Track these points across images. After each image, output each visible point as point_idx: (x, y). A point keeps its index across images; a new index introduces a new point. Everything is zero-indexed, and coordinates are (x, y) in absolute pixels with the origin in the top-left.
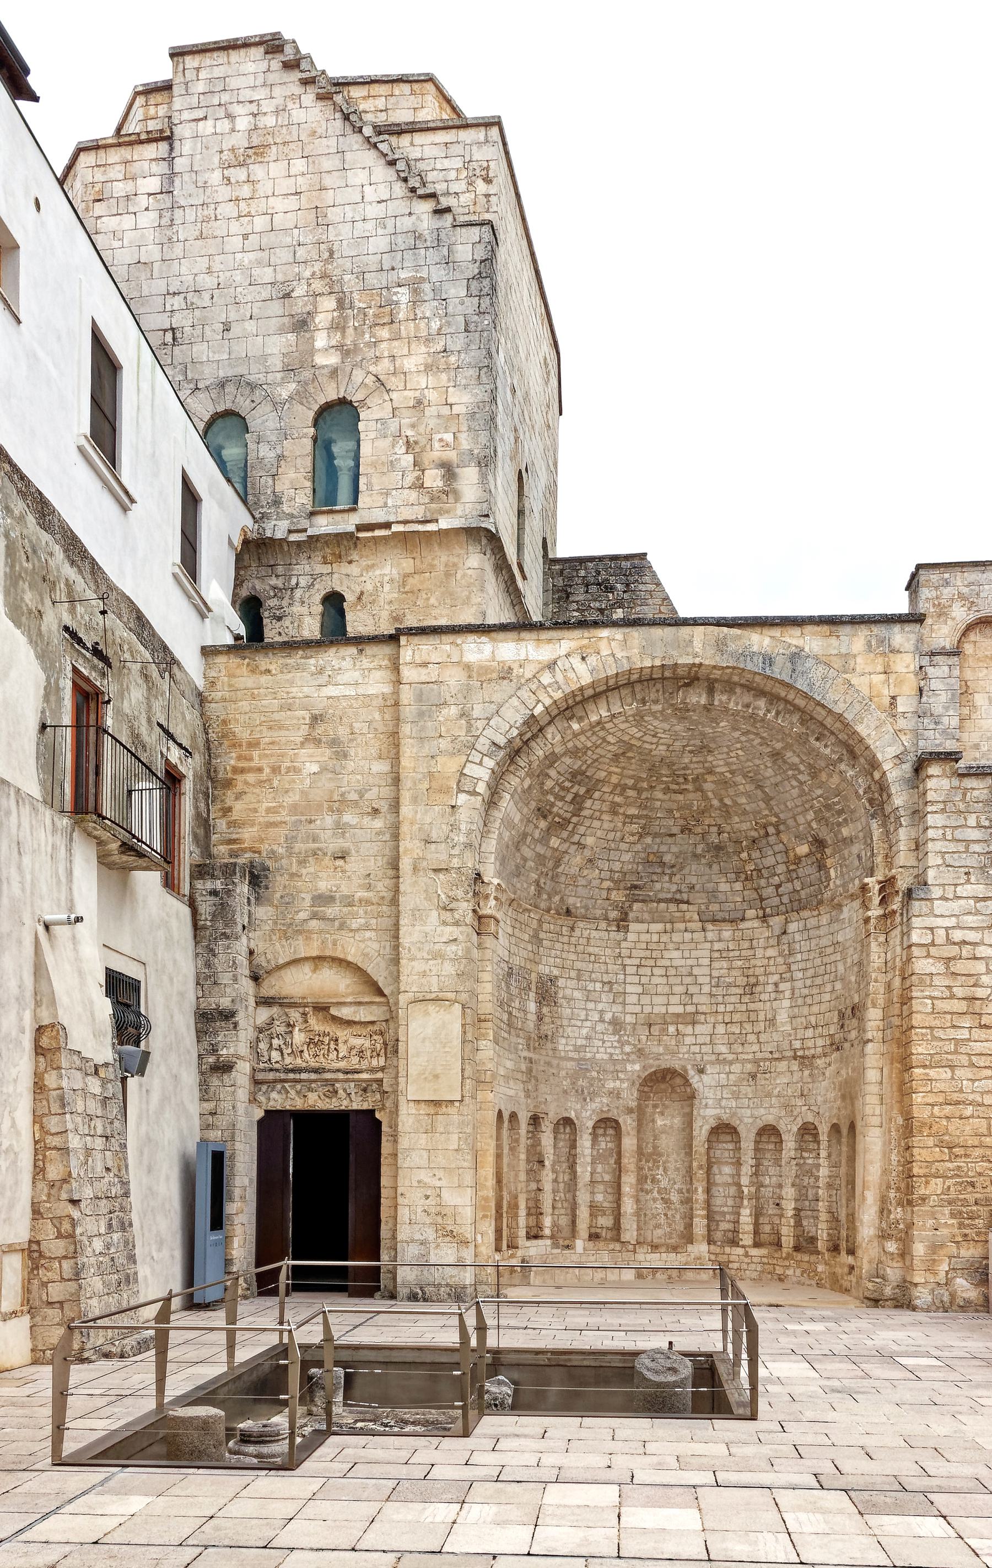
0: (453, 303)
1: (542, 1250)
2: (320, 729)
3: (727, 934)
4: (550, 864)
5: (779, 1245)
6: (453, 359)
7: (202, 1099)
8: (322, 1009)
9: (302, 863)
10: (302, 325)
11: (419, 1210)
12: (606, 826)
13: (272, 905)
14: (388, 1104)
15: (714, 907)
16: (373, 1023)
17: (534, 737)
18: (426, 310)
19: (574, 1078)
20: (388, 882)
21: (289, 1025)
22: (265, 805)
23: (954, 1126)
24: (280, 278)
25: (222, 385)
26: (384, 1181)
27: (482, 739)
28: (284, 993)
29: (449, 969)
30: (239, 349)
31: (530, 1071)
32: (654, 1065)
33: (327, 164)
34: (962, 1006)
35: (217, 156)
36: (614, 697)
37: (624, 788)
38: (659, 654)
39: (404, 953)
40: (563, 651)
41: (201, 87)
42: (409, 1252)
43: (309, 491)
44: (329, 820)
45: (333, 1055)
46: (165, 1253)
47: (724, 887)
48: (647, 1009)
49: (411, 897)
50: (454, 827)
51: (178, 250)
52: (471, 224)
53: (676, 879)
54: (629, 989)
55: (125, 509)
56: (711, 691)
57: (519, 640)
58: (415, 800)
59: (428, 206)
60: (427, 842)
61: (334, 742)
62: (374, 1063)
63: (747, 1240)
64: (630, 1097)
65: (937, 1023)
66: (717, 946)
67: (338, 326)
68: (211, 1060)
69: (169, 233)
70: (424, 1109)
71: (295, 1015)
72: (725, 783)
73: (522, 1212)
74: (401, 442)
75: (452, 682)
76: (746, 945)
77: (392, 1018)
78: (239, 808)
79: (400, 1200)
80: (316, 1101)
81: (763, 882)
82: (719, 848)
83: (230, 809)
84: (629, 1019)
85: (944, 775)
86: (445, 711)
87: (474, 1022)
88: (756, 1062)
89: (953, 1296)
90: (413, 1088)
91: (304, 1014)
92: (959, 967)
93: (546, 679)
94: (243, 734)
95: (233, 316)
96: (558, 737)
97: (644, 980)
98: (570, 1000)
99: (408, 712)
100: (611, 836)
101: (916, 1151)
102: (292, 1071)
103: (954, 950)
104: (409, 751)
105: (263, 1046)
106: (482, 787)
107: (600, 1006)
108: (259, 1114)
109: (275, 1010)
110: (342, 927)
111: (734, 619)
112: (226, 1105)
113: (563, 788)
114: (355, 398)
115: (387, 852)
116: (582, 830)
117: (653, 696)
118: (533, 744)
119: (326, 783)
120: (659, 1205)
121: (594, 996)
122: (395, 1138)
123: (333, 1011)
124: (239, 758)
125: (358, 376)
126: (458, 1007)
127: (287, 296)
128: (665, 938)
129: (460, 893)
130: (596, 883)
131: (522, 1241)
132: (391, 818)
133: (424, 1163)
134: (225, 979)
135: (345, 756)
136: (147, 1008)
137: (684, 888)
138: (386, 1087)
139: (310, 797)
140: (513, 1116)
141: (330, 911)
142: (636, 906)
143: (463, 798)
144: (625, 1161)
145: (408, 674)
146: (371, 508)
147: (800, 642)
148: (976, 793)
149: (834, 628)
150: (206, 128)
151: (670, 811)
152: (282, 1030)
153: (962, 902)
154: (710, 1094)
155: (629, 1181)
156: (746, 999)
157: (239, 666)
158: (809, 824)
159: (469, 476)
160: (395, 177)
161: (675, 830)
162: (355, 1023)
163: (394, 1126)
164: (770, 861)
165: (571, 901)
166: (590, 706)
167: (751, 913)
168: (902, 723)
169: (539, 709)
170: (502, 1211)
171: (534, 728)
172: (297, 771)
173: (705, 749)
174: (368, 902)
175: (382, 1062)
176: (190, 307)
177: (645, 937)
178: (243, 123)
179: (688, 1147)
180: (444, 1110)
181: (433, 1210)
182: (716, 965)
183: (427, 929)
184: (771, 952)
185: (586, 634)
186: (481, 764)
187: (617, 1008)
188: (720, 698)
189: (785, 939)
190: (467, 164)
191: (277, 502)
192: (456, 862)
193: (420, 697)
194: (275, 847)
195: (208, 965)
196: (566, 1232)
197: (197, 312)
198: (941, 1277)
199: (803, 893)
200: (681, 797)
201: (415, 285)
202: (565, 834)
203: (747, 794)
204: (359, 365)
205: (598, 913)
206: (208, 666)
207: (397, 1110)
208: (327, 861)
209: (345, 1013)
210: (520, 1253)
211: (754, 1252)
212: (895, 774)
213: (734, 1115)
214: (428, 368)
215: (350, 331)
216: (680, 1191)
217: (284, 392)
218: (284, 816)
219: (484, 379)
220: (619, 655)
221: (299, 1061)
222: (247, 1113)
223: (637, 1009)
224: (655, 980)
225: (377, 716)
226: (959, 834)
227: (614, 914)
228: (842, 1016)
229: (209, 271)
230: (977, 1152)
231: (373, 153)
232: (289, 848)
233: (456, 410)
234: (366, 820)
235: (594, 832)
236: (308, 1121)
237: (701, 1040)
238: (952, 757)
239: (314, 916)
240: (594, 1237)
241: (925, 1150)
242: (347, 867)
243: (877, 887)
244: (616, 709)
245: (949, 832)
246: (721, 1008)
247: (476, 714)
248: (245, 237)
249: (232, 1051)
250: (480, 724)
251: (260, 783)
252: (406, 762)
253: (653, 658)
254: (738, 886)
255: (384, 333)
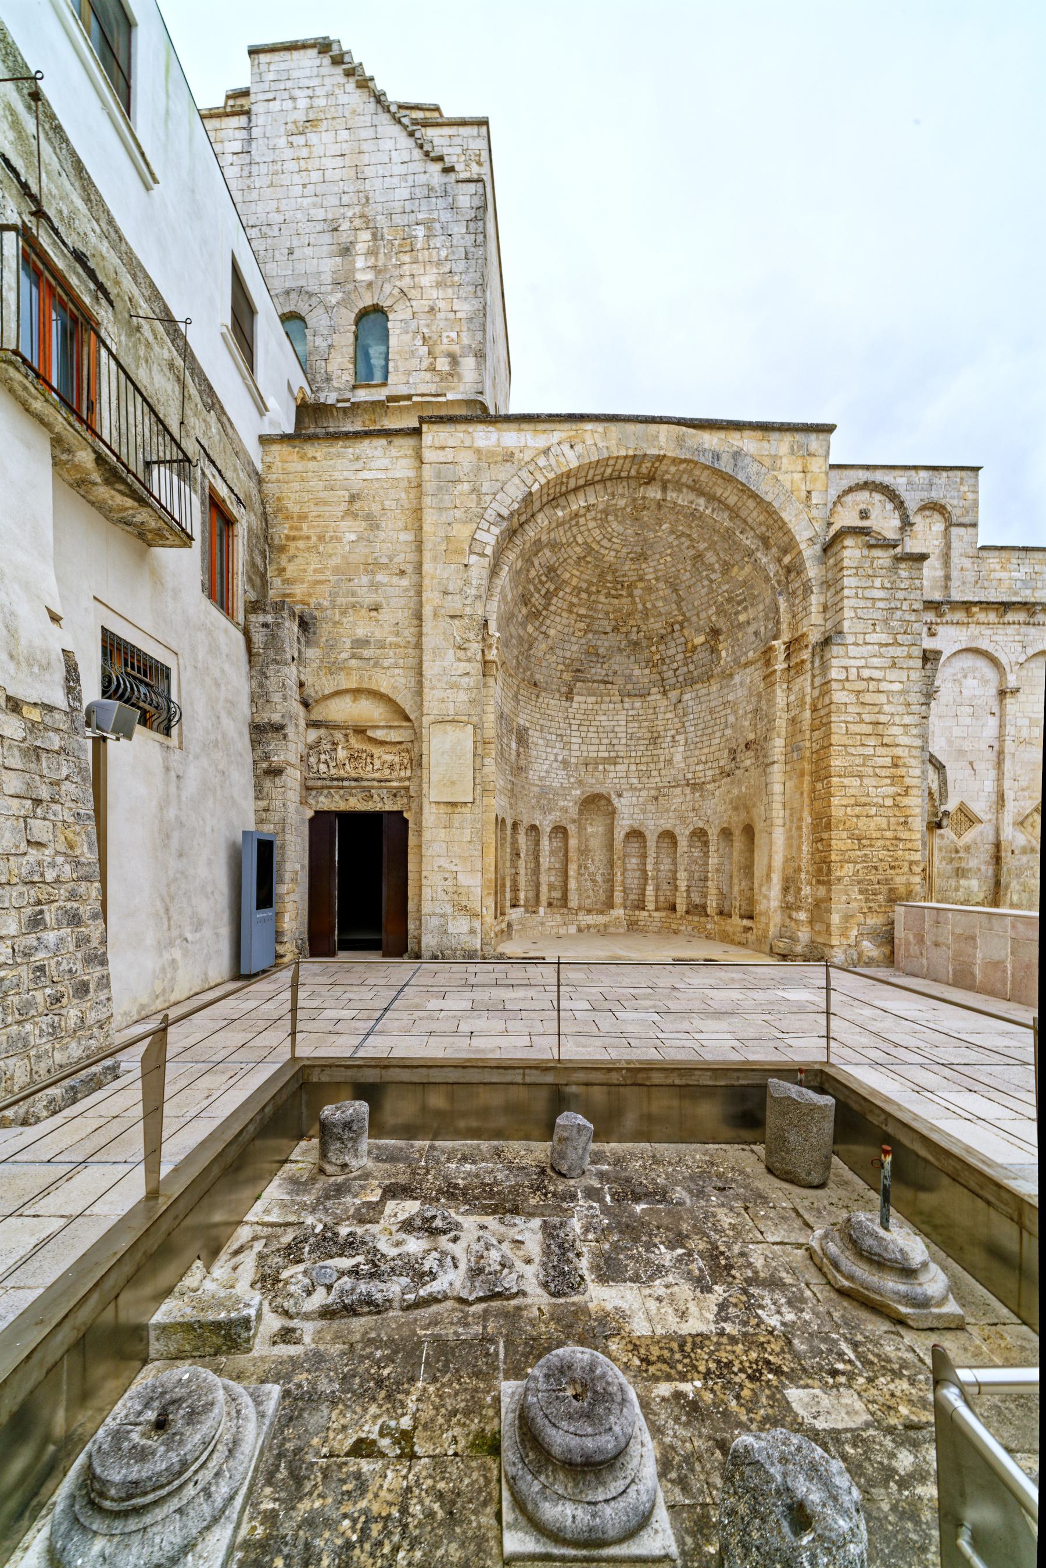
0: (455, 238)
1: (519, 915)
2: (357, 505)
3: (638, 705)
4: (526, 646)
5: (673, 908)
6: (456, 278)
7: (257, 798)
8: (360, 731)
9: (344, 613)
10: (346, 251)
11: (440, 889)
12: (564, 621)
13: (318, 647)
14: (414, 806)
15: (629, 687)
16: (401, 743)
17: (527, 521)
18: (437, 242)
19: (539, 799)
20: (412, 630)
21: (334, 743)
22: (313, 567)
23: (862, 822)
24: (330, 216)
25: (287, 293)
26: (411, 866)
27: (489, 511)
28: (330, 718)
29: (463, 697)
30: (301, 268)
31: (512, 790)
32: (589, 791)
33: (365, 134)
34: (869, 729)
35: (283, 127)
36: (590, 490)
37: (580, 590)
38: (632, 445)
39: (426, 683)
40: (555, 440)
41: (271, 76)
42: (431, 923)
43: (352, 372)
44: (365, 580)
45: (369, 768)
46: (207, 932)
47: (637, 672)
48: (585, 754)
49: (433, 634)
50: (467, 582)
51: (254, 195)
52: (469, 181)
53: (605, 666)
54: (574, 740)
55: (148, 188)
56: (664, 489)
57: (520, 430)
58: (435, 559)
59: (437, 167)
60: (446, 593)
61: (369, 517)
62: (402, 774)
63: (651, 906)
64: (574, 812)
65: (850, 742)
66: (631, 713)
67: (372, 252)
68: (265, 765)
69: (248, 182)
70: (443, 809)
71: (338, 736)
72: (649, 590)
73: (508, 890)
74: (419, 337)
75: (466, 464)
76: (651, 711)
77: (417, 738)
78: (291, 570)
79: (424, 882)
80: (356, 804)
81: (665, 668)
82: (636, 644)
83: (284, 570)
84: (574, 760)
85: (857, 546)
86: (459, 487)
87: (481, 744)
88: (658, 789)
89: (860, 955)
90: (435, 791)
91: (346, 735)
92: (868, 698)
93: (542, 461)
94: (294, 509)
95: (295, 243)
96: (546, 522)
97: (583, 734)
98: (536, 745)
99: (429, 487)
100: (566, 630)
101: (833, 842)
102: (337, 779)
103: (862, 685)
104: (430, 518)
105: (313, 760)
106: (489, 551)
107: (555, 751)
108: (310, 814)
109: (322, 732)
110: (376, 665)
111: (691, 420)
112: (277, 803)
113: (540, 581)
114: (385, 304)
115: (412, 605)
116: (548, 622)
117: (620, 491)
118: (526, 527)
119: (362, 549)
120: (589, 883)
121: (551, 743)
122: (419, 833)
123: (370, 733)
124: (291, 528)
125: (388, 288)
126: (470, 727)
127: (336, 230)
128: (596, 707)
129: (471, 636)
130: (554, 665)
131: (508, 910)
132: (415, 578)
133: (443, 852)
134: (276, 698)
135: (378, 527)
136: (180, 697)
137: (610, 673)
138: (412, 793)
139: (350, 560)
140: (503, 820)
141: (366, 653)
142: (579, 684)
143: (474, 558)
144: (570, 854)
145: (428, 455)
146: (397, 385)
147: (740, 444)
148: (881, 561)
149: (766, 434)
150: (275, 106)
151: (607, 613)
152: (328, 747)
153: (869, 647)
154: (625, 810)
155: (573, 868)
156: (651, 747)
157: (290, 454)
158: (709, 617)
159: (468, 364)
160: (414, 145)
161: (609, 629)
162: (386, 743)
163: (419, 823)
164: (672, 651)
165: (537, 676)
166: (571, 498)
167: (654, 690)
168: (815, 513)
169: (536, 487)
170: (498, 888)
171: (529, 507)
172: (339, 540)
173: (643, 557)
174: (398, 646)
175: (408, 773)
176: (264, 236)
177: (583, 706)
178: (302, 103)
179: (610, 846)
180: (459, 810)
181: (450, 890)
182: (630, 725)
183: (446, 664)
184: (669, 715)
185: (574, 427)
186: (488, 531)
187: (566, 753)
188: (671, 495)
189: (680, 706)
190: (464, 152)
191: (328, 379)
192: (468, 611)
193: (438, 475)
194: (321, 601)
195: (261, 685)
196: (532, 902)
197: (269, 240)
198: (852, 940)
199: (695, 673)
200: (616, 601)
201: (428, 224)
202: (537, 624)
203: (664, 599)
204: (389, 280)
205: (554, 687)
206: (265, 453)
207: (421, 809)
208: (364, 612)
209: (379, 734)
210: (507, 918)
211: (655, 914)
212: (809, 553)
213: (642, 824)
214: (439, 285)
215: (381, 256)
216: (603, 875)
217: (333, 299)
218: (328, 575)
219: (479, 294)
220: (600, 445)
221: (342, 772)
222: (297, 811)
223: (579, 754)
224: (590, 735)
225: (403, 495)
226: (868, 593)
227: (564, 689)
228: (733, 752)
229: (278, 211)
230: (880, 843)
231: (398, 127)
232: (333, 601)
233: (459, 315)
234: (395, 580)
235: (557, 624)
236: (349, 820)
237: (619, 775)
238: (864, 532)
239: (353, 656)
240: (550, 904)
241: (839, 841)
242: (380, 617)
243: (783, 647)
244: (592, 500)
245: (860, 591)
246: (633, 754)
247: (484, 490)
248: (304, 186)
249: (282, 758)
250: (488, 498)
251: (308, 549)
252: (427, 528)
253: (627, 449)
254: (647, 671)
255: (406, 258)
